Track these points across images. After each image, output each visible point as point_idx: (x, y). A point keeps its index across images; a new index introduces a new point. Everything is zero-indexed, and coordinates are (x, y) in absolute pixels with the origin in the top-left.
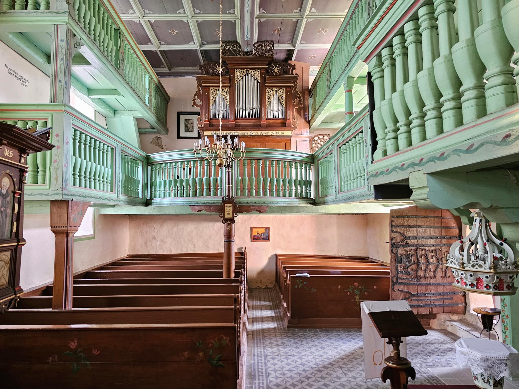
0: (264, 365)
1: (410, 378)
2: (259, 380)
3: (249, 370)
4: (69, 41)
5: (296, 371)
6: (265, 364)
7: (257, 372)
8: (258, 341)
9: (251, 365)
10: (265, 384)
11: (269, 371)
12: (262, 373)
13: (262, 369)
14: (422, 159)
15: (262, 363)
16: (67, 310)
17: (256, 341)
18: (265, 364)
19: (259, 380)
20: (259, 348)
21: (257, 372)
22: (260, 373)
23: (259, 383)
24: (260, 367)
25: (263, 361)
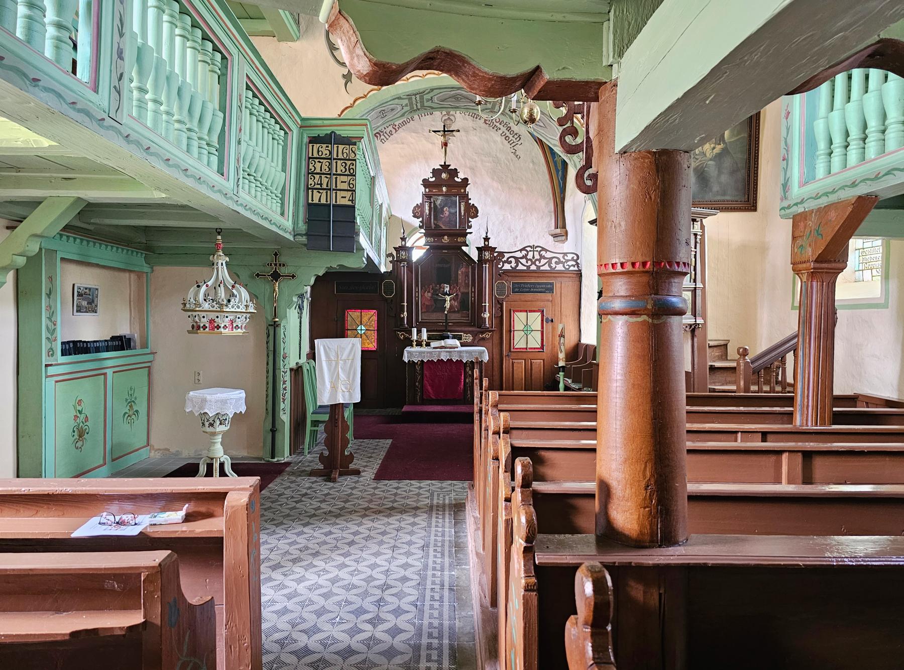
0: (431, 564)
1: (464, 248)
2: (443, 541)
3: (461, 556)
4: (783, 152)
5: (342, 595)
6: (426, 567)
7: (446, 553)
8: (435, 642)
9: (459, 564)
10: (433, 533)
11: (420, 553)
12: (435, 551)
13: (435, 556)
14: (115, 87)
15: (434, 569)
16: (688, 463)
17: (446, 641)
18: (426, 567)
19: (443, 541)
20: (436, 623)
21: (446, 553)
22: (434, 657)
23: (443, 535)
24: (440, 521)
25: (430, 573)
